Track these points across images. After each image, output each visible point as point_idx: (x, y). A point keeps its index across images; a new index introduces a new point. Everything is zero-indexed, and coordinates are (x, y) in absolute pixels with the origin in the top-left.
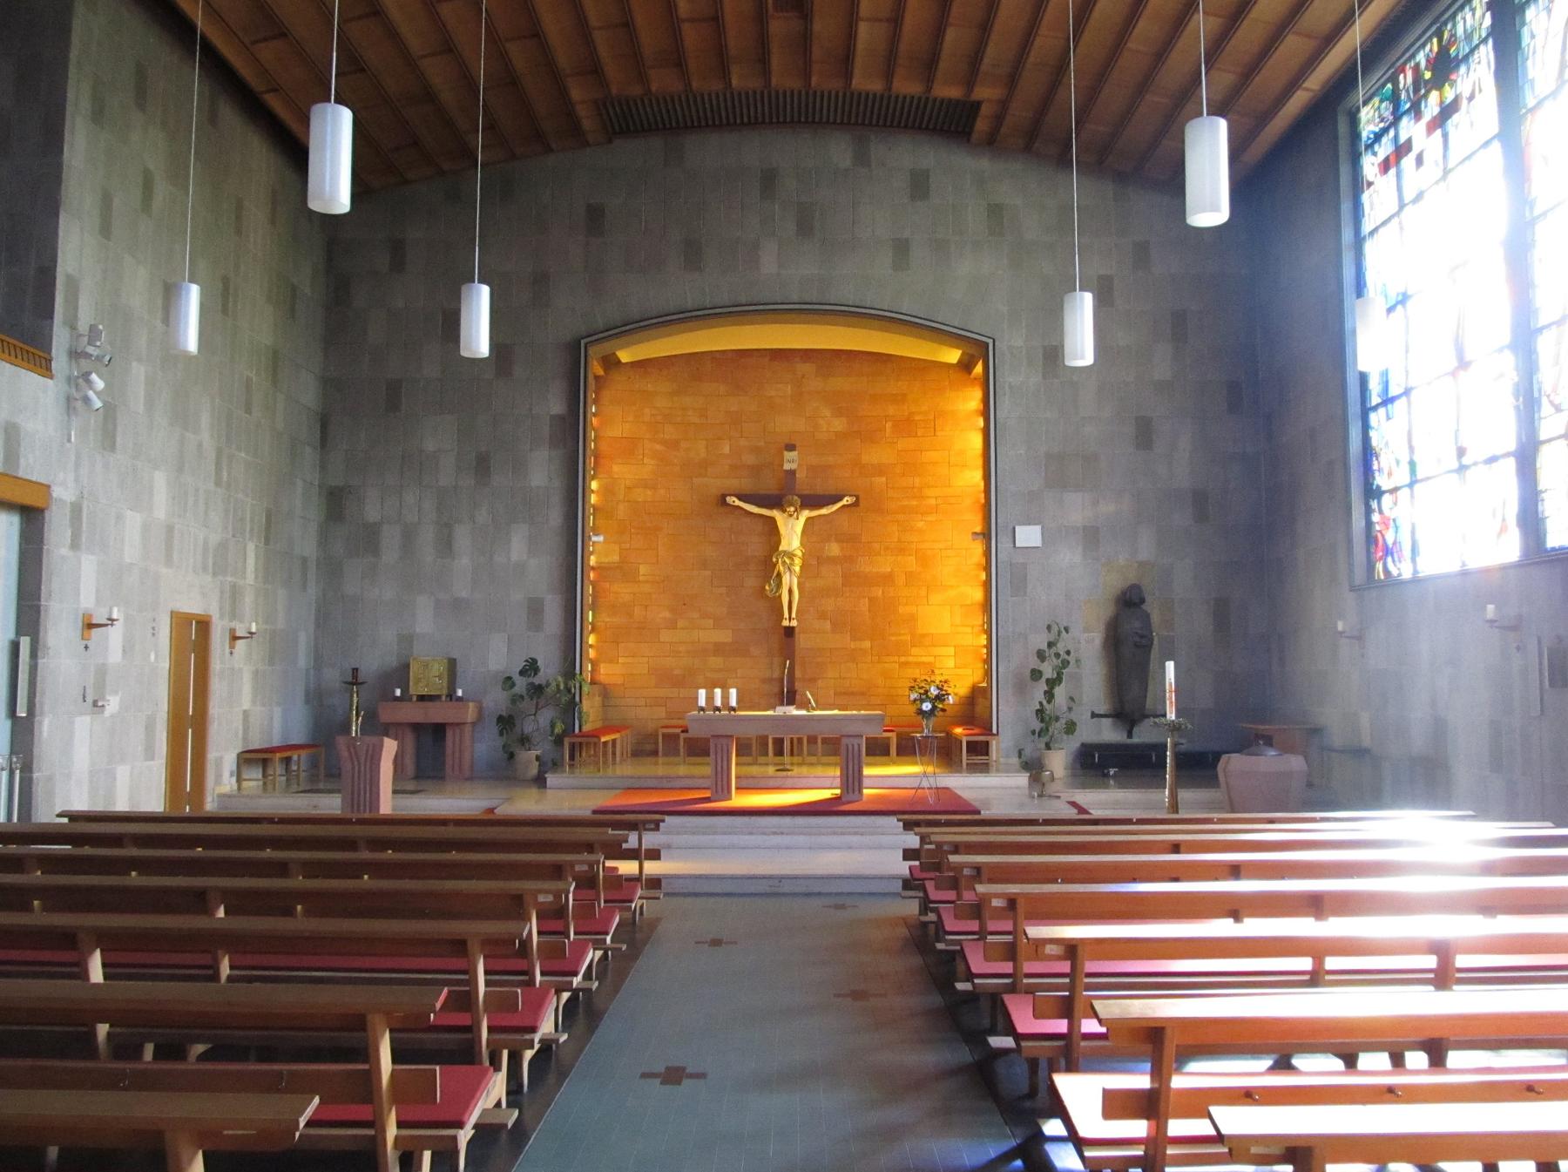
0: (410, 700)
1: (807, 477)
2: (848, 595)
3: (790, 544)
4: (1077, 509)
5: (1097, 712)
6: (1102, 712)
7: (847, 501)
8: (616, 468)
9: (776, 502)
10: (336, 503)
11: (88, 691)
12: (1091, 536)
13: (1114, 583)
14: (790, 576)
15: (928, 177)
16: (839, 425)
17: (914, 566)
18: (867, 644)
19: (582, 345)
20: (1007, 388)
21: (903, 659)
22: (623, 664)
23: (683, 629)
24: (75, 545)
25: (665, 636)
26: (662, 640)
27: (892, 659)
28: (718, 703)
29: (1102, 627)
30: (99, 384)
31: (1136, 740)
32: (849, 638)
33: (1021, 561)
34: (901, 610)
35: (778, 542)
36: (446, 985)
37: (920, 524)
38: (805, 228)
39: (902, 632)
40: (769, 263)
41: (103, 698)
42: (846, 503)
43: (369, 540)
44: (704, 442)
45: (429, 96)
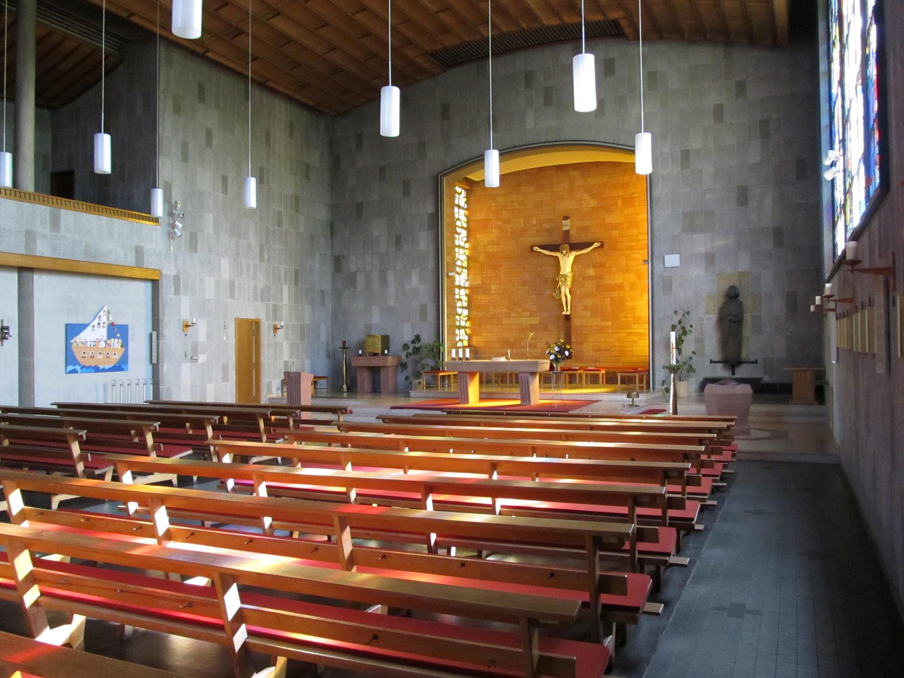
0: (366, 356)
1: (577, 233)
2: (599, 296)
3: (565, 271)
4: (701, 243)
5: (713, 360)
6: (716, 360)
7: (596, 245)
8: (479, 236)
9: (555, 248)
10: (338, 262)
11: (188, 353)
12: (710, 259)
13: (725, 286)
14: (565, 288)
15: (614, 62)
16: (593, 203)
18: (610, 323)
19: (439, 177)
20: (660, 177)
21: (628, 331)
22: (484, 336)
23: (514, 317)
24: (177, 292)
25: (505, 321)
26: (503, 324)
28: (461, 356)
29: (716, 311)
30: (180, 225)
34: (628, 304)
36: (356, 487)
37: (637, 256)
38: (548, 101)
39: (629, 316)
40: (530, 124)
41: (197, 355)
43: (351, 280)
44: (523, 218)
45: (337, 70)
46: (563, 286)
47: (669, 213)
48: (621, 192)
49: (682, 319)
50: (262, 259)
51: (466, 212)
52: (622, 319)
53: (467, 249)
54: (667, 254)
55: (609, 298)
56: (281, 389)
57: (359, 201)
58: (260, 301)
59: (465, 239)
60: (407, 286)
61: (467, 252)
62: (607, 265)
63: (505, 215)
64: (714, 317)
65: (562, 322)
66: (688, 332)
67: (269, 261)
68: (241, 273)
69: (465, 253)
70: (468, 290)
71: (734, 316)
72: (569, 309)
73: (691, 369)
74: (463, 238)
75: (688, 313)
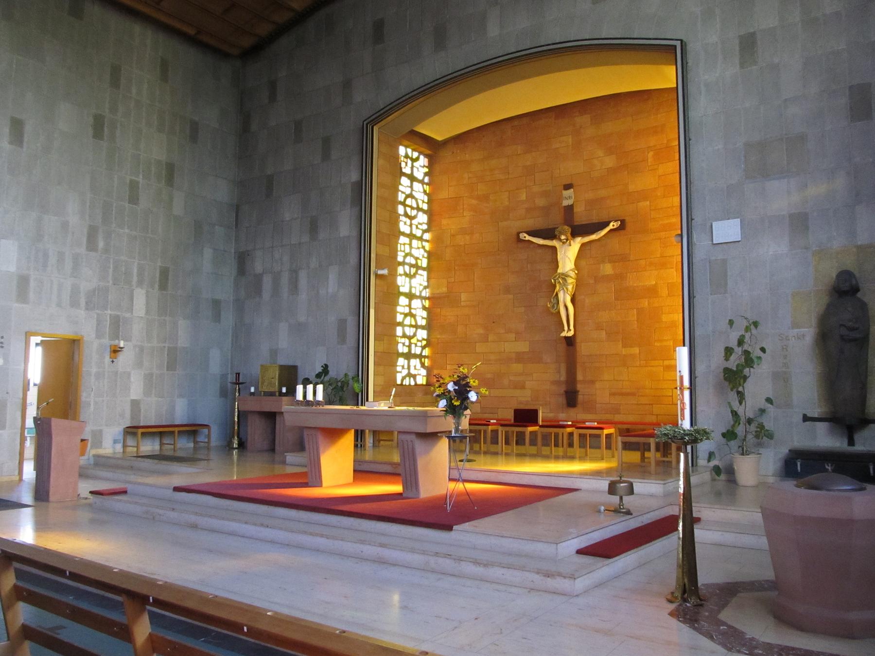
3: (564, 266)
6: (816, 416)
8: (444, 222)
9: (550, 234)
10: (242, 260)
13: (830, 271)
16: (610, 162)
17: (675, 278)
18: (636, 350)
21: (666, 363)
25: (480, 348)
27: (656, 363)
29: (814, 322)
31: (860, 447)
32: (621, 345)
33: (720, 257)
34: (665, 318)
35: (557, 267)
40: (493, 30)
42: (612, 228)
43: (256, 287)
46: (562, 292)
47: (720, 146)
48: (653, 141)
49: (743, 336)
50: (91, 245)
51: (427, 188)
52: (656, 344)
53: (427, 241)
54: (717, 220)
55: (635, 310)
56: (122, 441)
57: (269, 173)
58: (84, 308)
59: (425, 227)
60: (322, 292)
61: (427, 246)
62: (632, 258)
63: (482, 189)
64: (809, 333)
65: (563, 346)
66: (755, 360)
67: (106, 251)
68: (45, 266)
69: (423, 247)
70: (427, 301)
71: (852, 329)
72: (572, 327)
73: (763, 434)
74: (421, 224)
75: (756, 324)
